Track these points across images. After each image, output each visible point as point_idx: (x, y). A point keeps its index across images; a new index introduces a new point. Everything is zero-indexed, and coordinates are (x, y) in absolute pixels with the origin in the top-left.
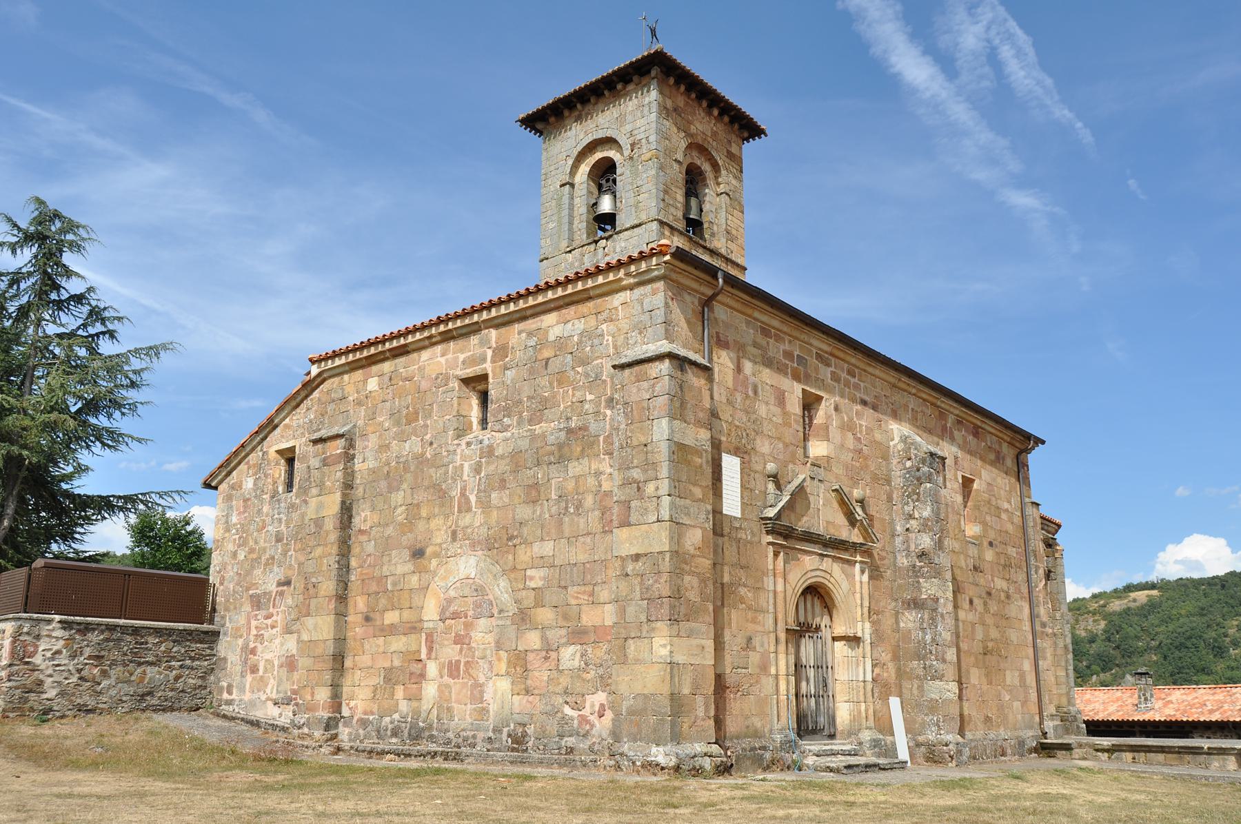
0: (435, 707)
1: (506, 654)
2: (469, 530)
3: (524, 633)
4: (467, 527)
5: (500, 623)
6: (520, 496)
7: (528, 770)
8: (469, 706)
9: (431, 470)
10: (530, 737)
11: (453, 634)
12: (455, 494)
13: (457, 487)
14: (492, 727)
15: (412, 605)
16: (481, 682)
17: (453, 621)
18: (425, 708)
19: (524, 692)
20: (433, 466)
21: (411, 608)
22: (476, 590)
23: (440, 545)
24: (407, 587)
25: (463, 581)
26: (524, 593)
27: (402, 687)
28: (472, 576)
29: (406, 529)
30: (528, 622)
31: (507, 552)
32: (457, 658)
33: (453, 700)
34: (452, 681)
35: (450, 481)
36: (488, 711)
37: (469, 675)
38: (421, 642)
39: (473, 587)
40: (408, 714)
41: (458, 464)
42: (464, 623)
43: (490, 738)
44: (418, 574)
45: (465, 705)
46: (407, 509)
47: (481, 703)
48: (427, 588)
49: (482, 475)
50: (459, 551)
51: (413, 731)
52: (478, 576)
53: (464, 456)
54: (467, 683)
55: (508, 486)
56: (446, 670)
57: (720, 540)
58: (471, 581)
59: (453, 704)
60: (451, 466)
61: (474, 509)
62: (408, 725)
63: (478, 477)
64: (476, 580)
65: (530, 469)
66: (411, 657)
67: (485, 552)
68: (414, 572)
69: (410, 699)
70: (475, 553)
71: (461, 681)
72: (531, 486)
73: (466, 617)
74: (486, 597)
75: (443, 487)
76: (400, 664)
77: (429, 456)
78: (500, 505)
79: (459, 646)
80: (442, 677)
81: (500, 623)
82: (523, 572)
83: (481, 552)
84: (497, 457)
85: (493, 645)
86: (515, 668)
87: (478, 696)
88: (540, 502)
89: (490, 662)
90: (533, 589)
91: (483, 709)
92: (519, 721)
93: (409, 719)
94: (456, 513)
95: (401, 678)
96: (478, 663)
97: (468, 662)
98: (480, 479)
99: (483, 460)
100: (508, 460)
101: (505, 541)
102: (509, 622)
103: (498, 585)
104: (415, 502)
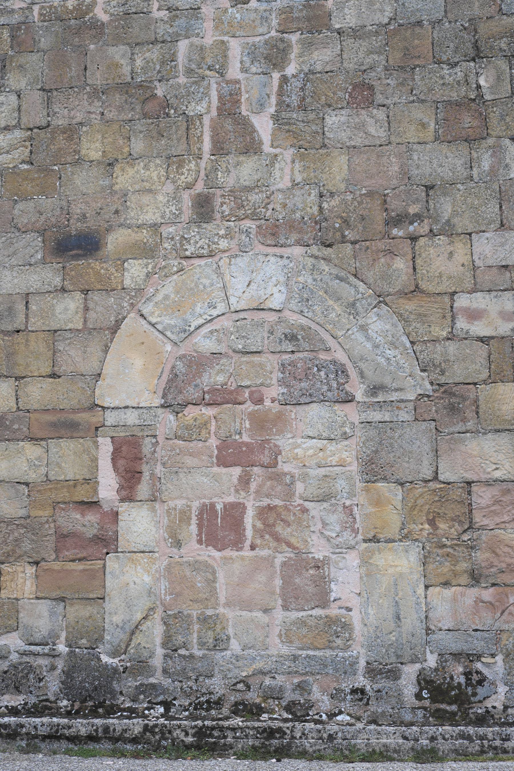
0: (158, 616)
1: (399, 492)
2: (255, 198)
3: (462, 441)
4: (248, 189)
5: (376, 416)
6: (424, 126)
7: (471, 706)
8: (279, 614)
9: (111, 50)
10: (493, 684)
11: (213, 442)
12: (201, 108)
13: (206, 94)
14: (362, 663)
15: (59, 370)
16: (319, 556)
17: (210, 412)
18: (117, 619)
19: (464, 579)
20: (118, 40)
21: (54, 376)
22: (292, 338)
23: (155, 227)
24: (35, 323)
25: (242, 315)
26: (452, 347)
27: (31, 570)
28: (276, 302)
29: (28, 187)
30: (470, 414)
31: (390, 253)
32: (231, 499)
33: (222, 599)
34: (217, 554)
35: (182, 80)
36: (347, 626)
37: (277, 538)
38: (95, 460)
39: (280, 331)
40: (54, 637)
41: (209, 40)
42: (252, 416)
43: (362, 691)
44: (78, 295)
45: (266, 611)
46: (31, 139)
47: (324, 604)
48: (115, 329)
49: (291, 70)
50: (223, 244)
51: (79, 677)
52: (293, 305)
53: (259, 278)
54: (269, 561)
55: (379, 98)
56: (194, 528)
57: (197, 169)
58: (272, 317)
59: (221, 610)
60: (183, 46)
61: (267, 148)
62: (60, 664)
63: (276, 76)
64: (287, 313)
65: (453, 65)
66: (63, 495)
67: (314, 250)
68: (63, 290)
69: (63, 599)
70: (278, 251)
71: (247, 553)
72: (458, 104)
73: (260, 401)
74: (323, 356)
75: (159, 92)
76: (22, 512)
77: (104, 18)
78: (358, 141)
79: (237, 471)
80: (178, 544)
81: (376, 416)
82: (447, 299)
83: (298, 251)
84: (339, 32)
85: (354, 467)
86: (432, 522)
87: (311, 589)
88: (491, 141)
89: (348, 510)
90: (481, 340)
91: (330, 621)
92: (455, 647)
93: (62, 648)
94: (206, 156)
95: (27, 546)
96: (305, 511)
97: (270, 508)
98: (284, 80)
99: (294, 38)
100: (377, 42)
101: (380, 227)
102: (404, 416)
103: (364, 328)
104: (60, 122)
